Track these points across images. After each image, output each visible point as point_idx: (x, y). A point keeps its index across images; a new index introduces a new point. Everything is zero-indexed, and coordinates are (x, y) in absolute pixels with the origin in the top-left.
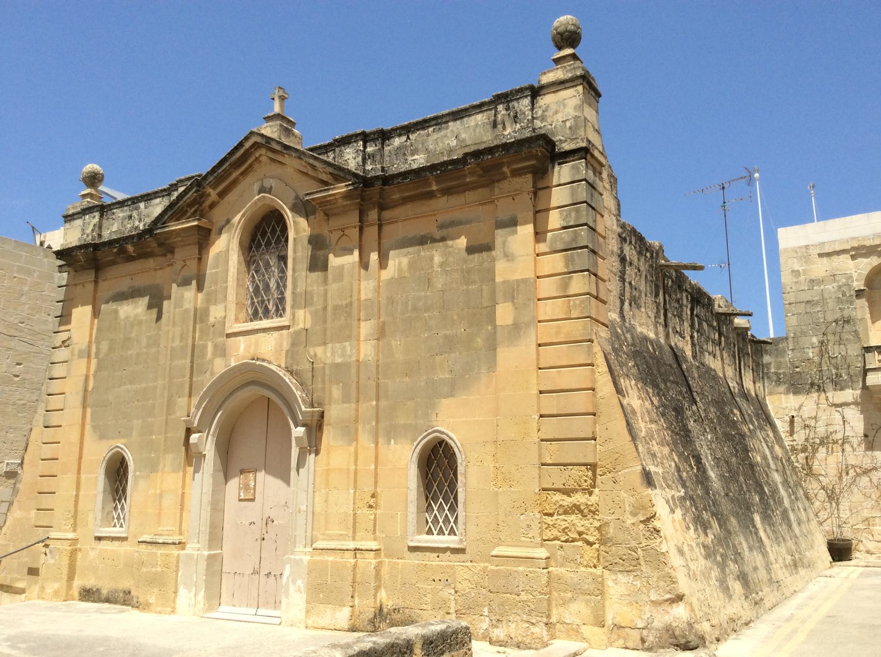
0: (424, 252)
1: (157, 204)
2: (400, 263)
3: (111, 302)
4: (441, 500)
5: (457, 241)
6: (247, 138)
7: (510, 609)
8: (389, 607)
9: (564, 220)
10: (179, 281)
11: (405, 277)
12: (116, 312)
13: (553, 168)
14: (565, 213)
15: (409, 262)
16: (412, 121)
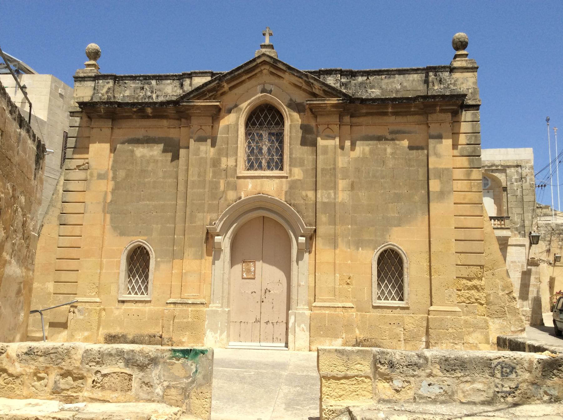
0: (380, 145)
1: (168, 84)
2: (364, 150)
3: (127, 144)
4: (386, 281)
5: (402, 142)
6: (259, 57)
7: (443, 337)
8: (361, 339)
9: (468, 140)
10: (195, 138)
11: (367, 158)
12: (132, 151)
13: (462, 112)
14: (468, 137)
15: (370, 149)
16: (372, 69)
